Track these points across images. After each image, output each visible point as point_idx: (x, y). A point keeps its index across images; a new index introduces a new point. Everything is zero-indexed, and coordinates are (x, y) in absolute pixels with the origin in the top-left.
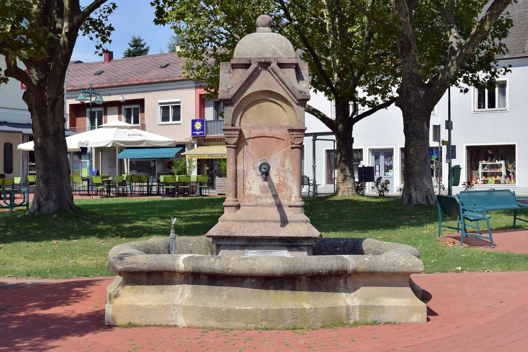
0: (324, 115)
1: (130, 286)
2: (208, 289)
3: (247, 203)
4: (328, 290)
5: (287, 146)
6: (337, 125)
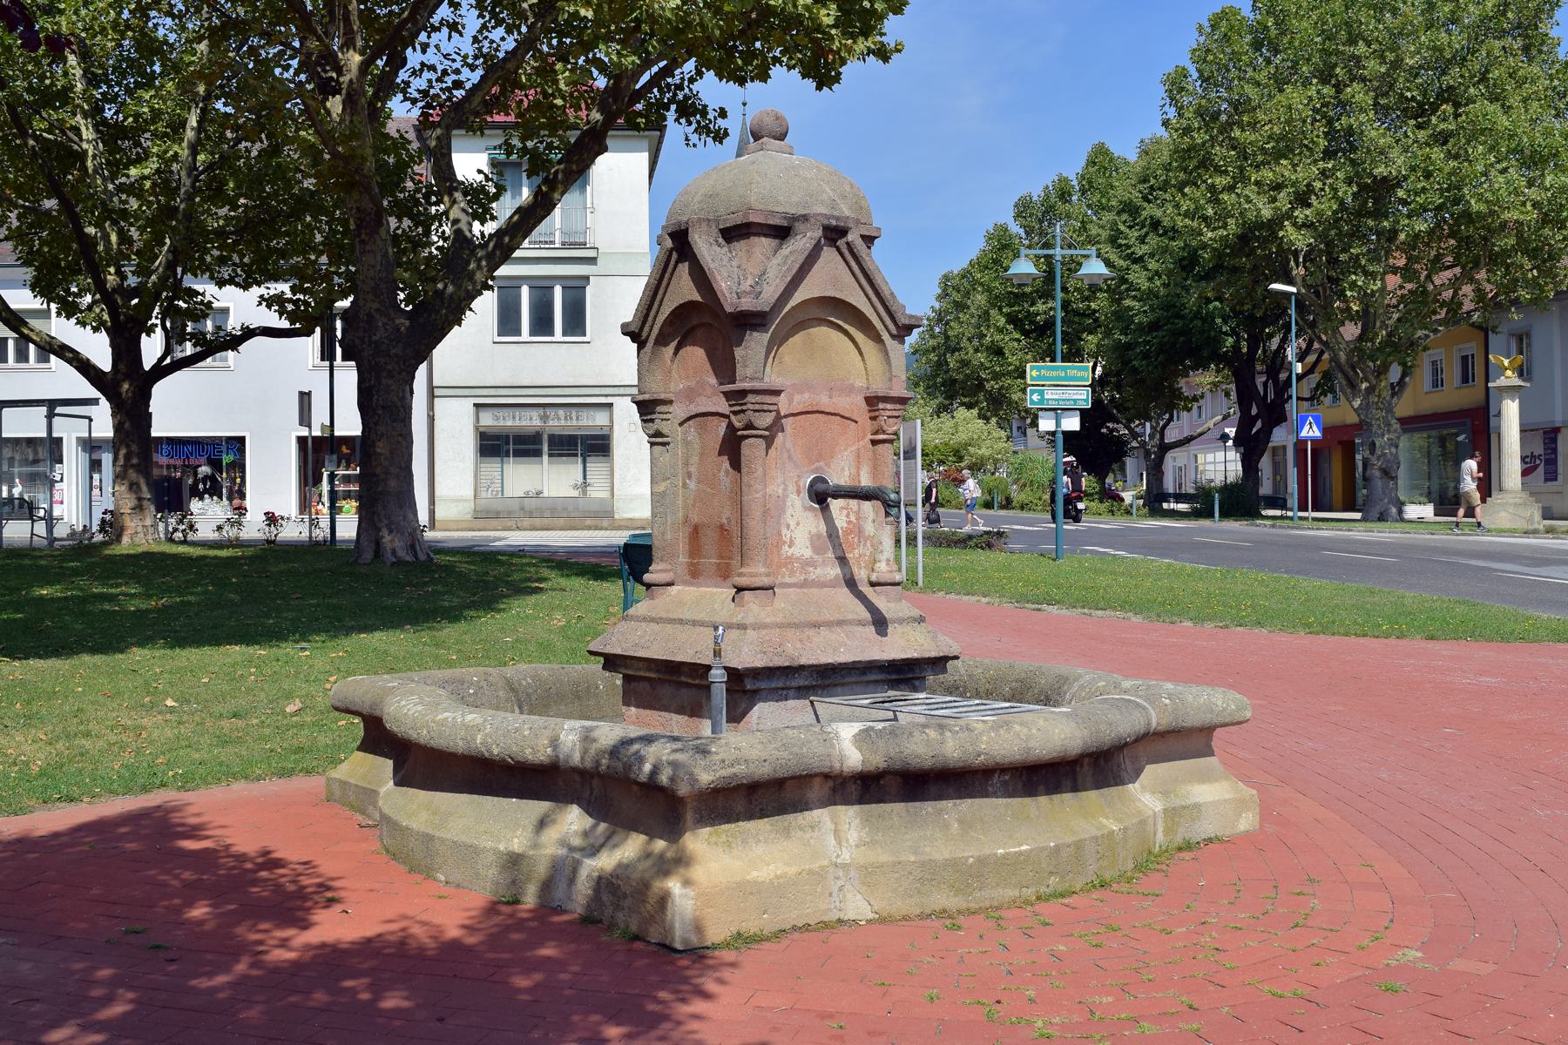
0: (88, 360)
1: (708, 829)
2: (908, 811)
3: (787, 580)
5: (863, 438)
6: (118, 385)
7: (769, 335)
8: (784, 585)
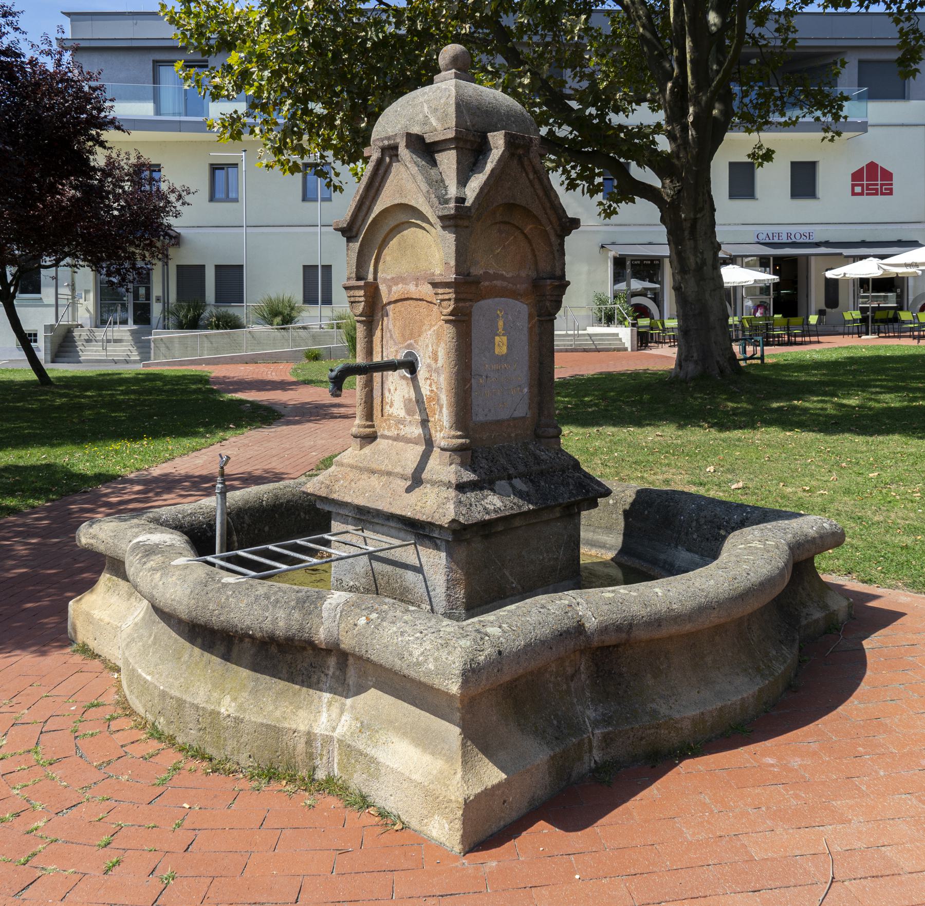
3: (386, 433)
4: (291, 679)
7: (359, 243)
8: (385, 437)
